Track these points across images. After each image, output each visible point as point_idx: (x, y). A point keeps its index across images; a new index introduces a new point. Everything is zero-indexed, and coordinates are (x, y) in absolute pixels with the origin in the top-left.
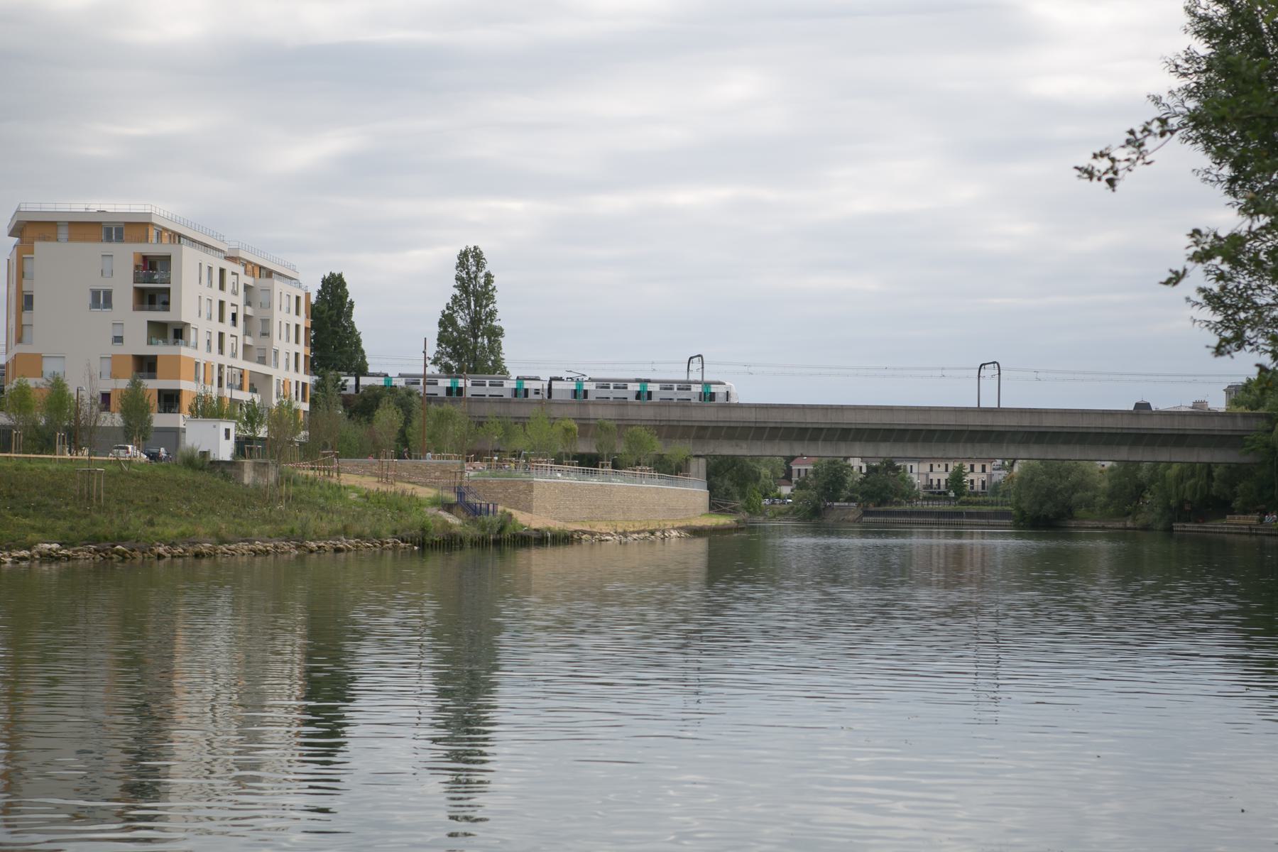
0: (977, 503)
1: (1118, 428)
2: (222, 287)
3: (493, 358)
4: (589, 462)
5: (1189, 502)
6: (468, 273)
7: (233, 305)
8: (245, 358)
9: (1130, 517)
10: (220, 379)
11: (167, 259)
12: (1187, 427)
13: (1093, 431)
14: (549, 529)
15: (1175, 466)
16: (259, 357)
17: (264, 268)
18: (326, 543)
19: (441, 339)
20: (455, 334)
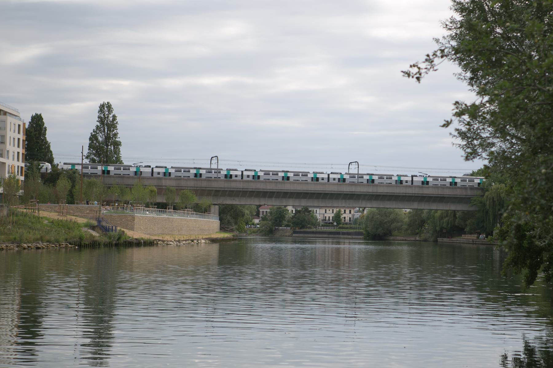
0: (347, 228)
1: (413, 194)
3: (116, 156)
4: (162, 207)
5: (445, 228)
6: (104, 115)
9: (418, 235)
13: (402, 194)
14: (142, 239)
15: (439, 212)
19: (90, 146)
20: (97, 144)
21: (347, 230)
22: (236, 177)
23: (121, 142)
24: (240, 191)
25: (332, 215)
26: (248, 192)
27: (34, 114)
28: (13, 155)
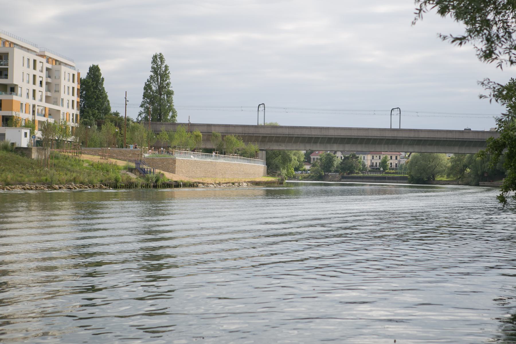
1: (453, 138)
2: (35, 68)
3: (169, 105)
4: (209, 151)
5: (487, 173)
7: (40, 77)
10: (34, 111)
11: (6, 55)
12: (485, 138)
13: (442, 139)
14: (182, 181)
16: (54, 102)
17: (58, 61)
19: (145, 96)
20: (151, 93)
23: (174, 91)
26: (294, 138)
27: (91, 66)
28: (68, 103)
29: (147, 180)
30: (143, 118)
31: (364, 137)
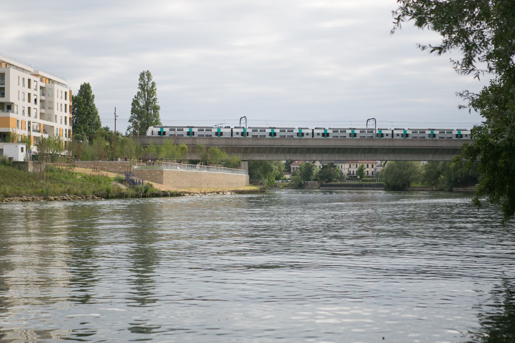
1: (427, 147)
2: (29, 87)
3: (155, 119)
5: (460, 179)
6: (144, 82)
7: (35, 95)
8: (41, 118)
9: (434, 185)
10: (29, 128)
12: (457, 146)
13: (417, 148)
14: (169, 191)
17: (51, 80)
18: (59, 197)
19: (133, 111)
20: (139, 109)
21: (369, 182)
22: (307, 135)
24: (267, 148)
25: (356, 170)
26: (300, 149)
29: (136, 190)
30: (132, 132)
31: (341, 147)
